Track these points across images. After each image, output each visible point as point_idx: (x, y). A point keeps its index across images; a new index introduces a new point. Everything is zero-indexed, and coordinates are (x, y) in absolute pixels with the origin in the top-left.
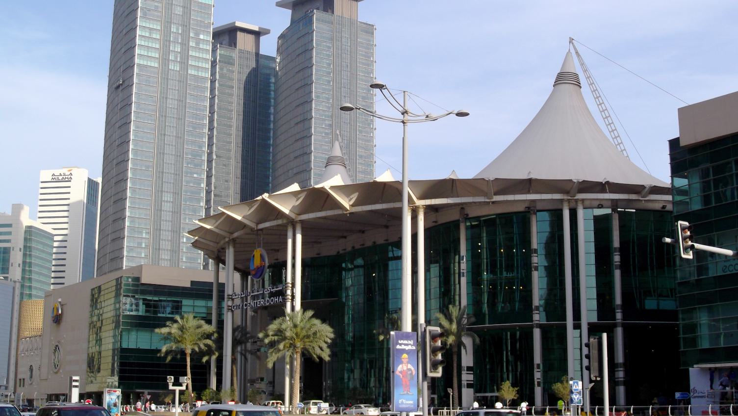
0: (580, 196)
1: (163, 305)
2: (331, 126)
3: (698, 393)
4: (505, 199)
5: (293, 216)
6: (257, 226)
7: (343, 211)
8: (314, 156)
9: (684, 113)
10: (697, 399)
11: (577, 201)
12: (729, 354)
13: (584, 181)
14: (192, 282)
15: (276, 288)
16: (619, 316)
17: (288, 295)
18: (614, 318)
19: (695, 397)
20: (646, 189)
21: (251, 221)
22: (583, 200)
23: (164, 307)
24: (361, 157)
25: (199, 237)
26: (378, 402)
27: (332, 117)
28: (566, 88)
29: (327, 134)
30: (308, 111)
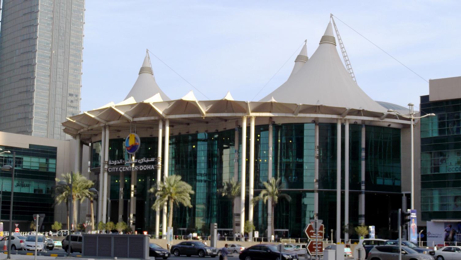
0: (348, 117)
1: (9, 160)
2: (52, 18)
3: (432, 235)
4: (305, 116)
5: (164, 115)
6: (133, 119)
7: (200, 115)
8: (39, 41)
9: (433, 83)
10: (430, 238)
11: (345, 120)
12: (455, 215)
13: (352, 109)
14: (30, 145)
15: (149, 160)
16: (363, 187)
17: (159, 165)
18: (360, 189)
19: (430, 237)
20: (384, 116)
21: (129, 116)
22: (349, 120)
23: (11, 162)
24: (73, 44)
25: (76, 121)
26: (275, 237)
27: (53, 11)
28: (327, 46)
29: (48, 24)
30: (35, 6)
